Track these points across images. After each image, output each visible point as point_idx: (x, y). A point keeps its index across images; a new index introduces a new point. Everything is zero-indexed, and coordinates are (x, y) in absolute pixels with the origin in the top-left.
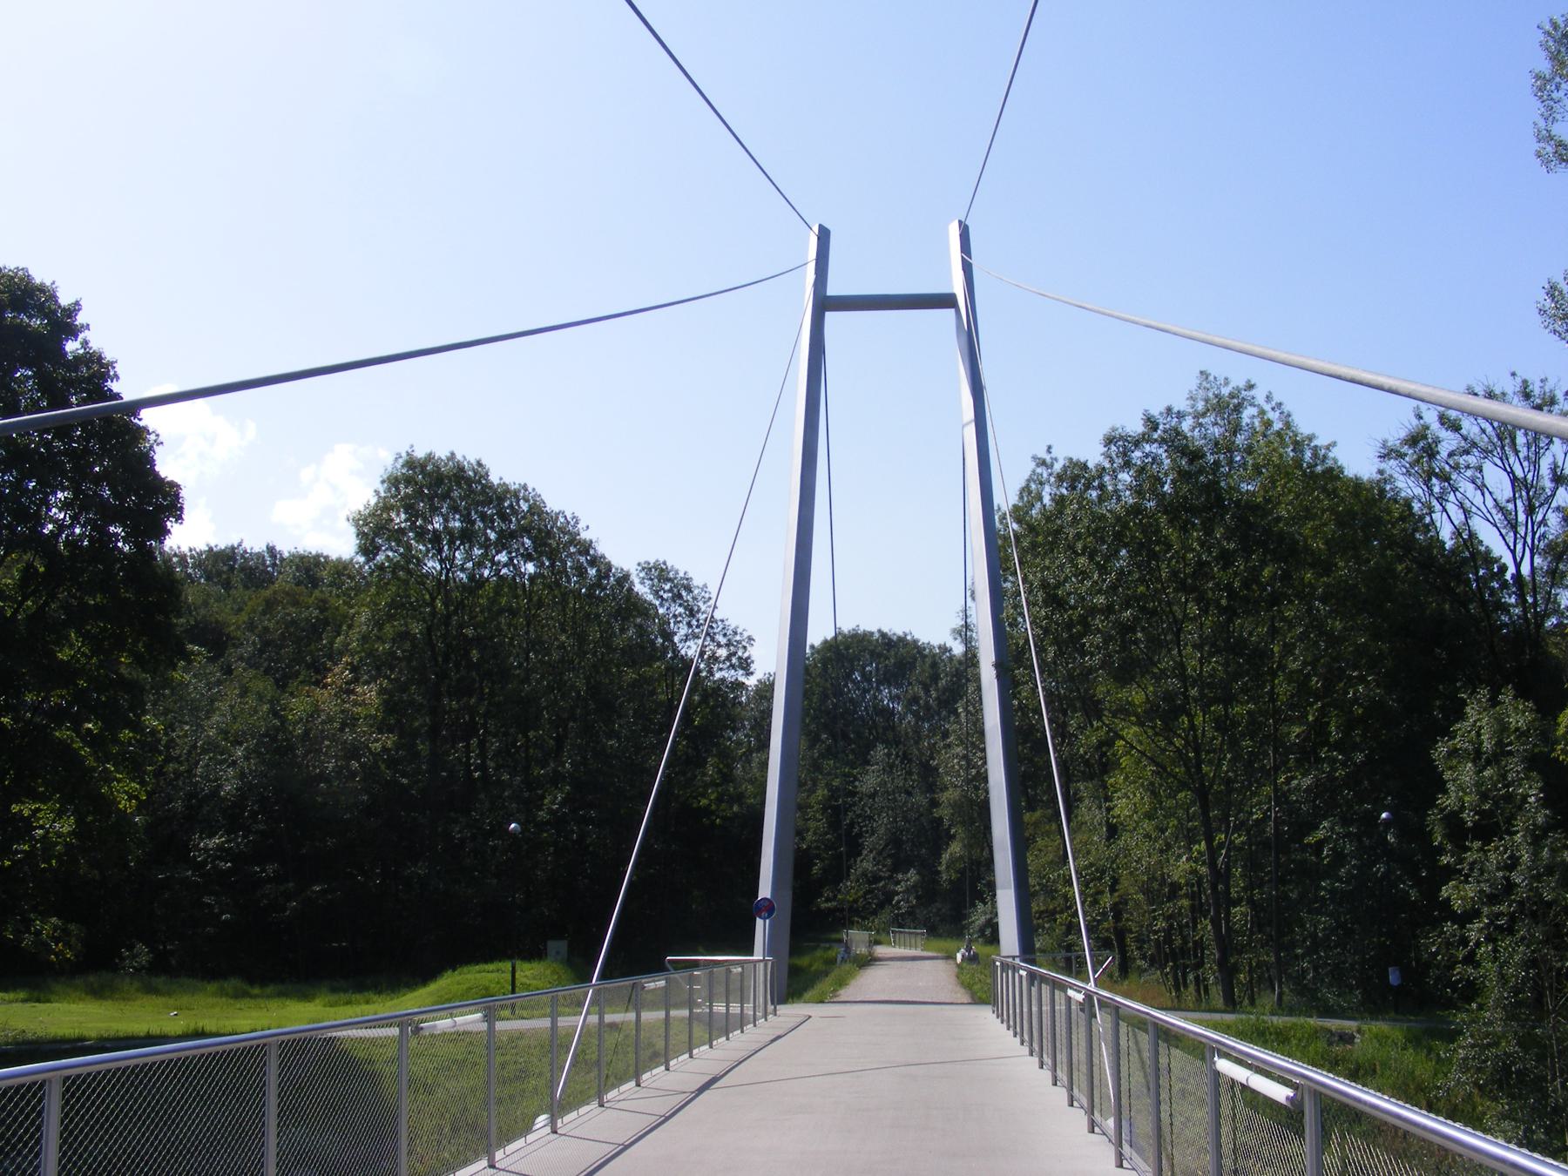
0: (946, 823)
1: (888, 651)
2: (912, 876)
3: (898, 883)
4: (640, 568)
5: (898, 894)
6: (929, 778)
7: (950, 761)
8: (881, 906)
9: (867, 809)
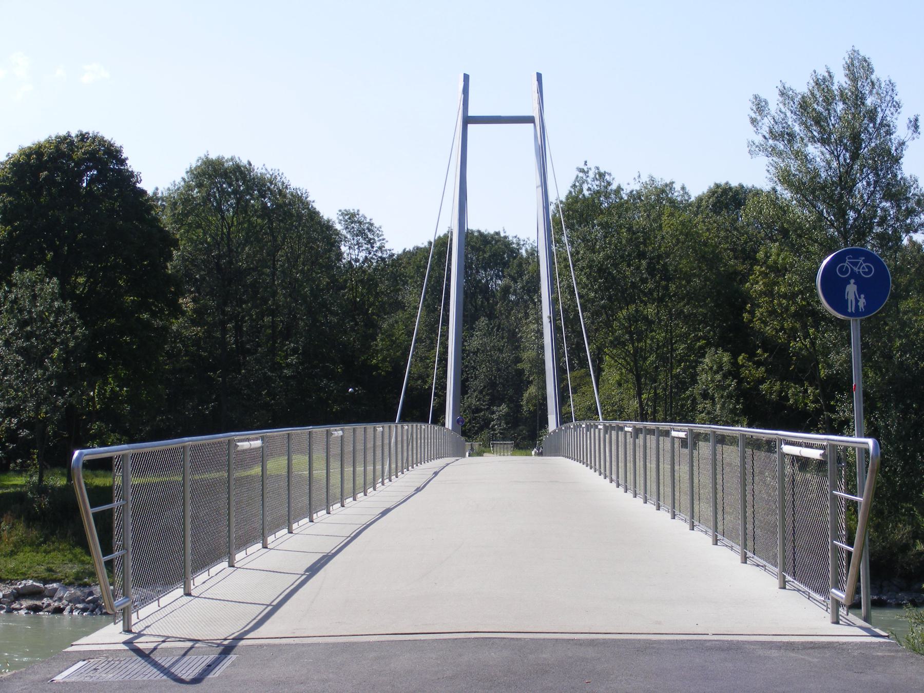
0: (527, 373)
1: (485, 247)
2: (504, 409)
3: (493, 413)
4: (340, 213)
5: (493, 420)
6: (514, 340)
7: (527, 332)
8: (481, 429)
9: (472, 362)
